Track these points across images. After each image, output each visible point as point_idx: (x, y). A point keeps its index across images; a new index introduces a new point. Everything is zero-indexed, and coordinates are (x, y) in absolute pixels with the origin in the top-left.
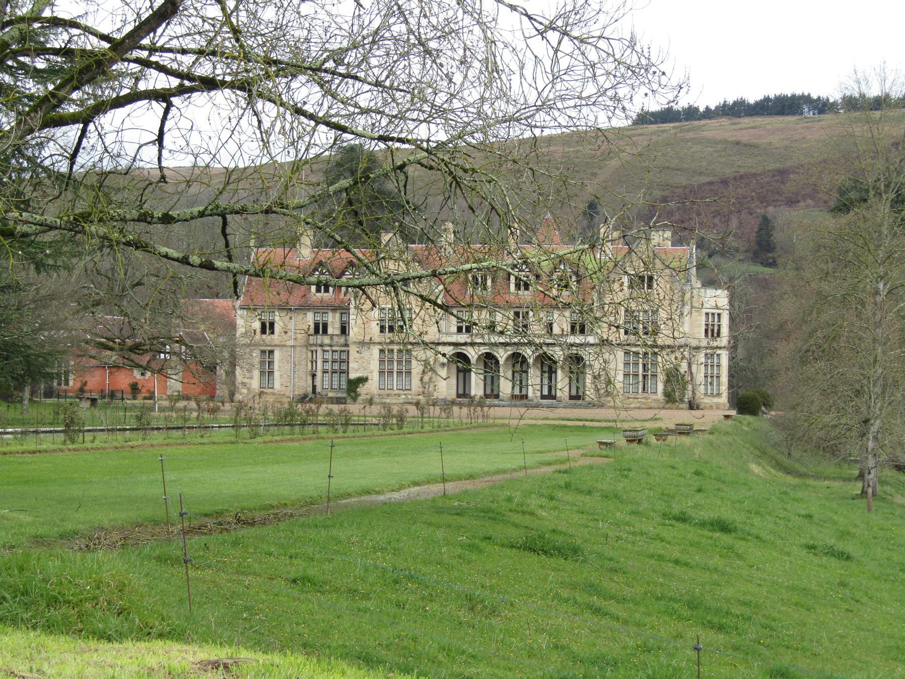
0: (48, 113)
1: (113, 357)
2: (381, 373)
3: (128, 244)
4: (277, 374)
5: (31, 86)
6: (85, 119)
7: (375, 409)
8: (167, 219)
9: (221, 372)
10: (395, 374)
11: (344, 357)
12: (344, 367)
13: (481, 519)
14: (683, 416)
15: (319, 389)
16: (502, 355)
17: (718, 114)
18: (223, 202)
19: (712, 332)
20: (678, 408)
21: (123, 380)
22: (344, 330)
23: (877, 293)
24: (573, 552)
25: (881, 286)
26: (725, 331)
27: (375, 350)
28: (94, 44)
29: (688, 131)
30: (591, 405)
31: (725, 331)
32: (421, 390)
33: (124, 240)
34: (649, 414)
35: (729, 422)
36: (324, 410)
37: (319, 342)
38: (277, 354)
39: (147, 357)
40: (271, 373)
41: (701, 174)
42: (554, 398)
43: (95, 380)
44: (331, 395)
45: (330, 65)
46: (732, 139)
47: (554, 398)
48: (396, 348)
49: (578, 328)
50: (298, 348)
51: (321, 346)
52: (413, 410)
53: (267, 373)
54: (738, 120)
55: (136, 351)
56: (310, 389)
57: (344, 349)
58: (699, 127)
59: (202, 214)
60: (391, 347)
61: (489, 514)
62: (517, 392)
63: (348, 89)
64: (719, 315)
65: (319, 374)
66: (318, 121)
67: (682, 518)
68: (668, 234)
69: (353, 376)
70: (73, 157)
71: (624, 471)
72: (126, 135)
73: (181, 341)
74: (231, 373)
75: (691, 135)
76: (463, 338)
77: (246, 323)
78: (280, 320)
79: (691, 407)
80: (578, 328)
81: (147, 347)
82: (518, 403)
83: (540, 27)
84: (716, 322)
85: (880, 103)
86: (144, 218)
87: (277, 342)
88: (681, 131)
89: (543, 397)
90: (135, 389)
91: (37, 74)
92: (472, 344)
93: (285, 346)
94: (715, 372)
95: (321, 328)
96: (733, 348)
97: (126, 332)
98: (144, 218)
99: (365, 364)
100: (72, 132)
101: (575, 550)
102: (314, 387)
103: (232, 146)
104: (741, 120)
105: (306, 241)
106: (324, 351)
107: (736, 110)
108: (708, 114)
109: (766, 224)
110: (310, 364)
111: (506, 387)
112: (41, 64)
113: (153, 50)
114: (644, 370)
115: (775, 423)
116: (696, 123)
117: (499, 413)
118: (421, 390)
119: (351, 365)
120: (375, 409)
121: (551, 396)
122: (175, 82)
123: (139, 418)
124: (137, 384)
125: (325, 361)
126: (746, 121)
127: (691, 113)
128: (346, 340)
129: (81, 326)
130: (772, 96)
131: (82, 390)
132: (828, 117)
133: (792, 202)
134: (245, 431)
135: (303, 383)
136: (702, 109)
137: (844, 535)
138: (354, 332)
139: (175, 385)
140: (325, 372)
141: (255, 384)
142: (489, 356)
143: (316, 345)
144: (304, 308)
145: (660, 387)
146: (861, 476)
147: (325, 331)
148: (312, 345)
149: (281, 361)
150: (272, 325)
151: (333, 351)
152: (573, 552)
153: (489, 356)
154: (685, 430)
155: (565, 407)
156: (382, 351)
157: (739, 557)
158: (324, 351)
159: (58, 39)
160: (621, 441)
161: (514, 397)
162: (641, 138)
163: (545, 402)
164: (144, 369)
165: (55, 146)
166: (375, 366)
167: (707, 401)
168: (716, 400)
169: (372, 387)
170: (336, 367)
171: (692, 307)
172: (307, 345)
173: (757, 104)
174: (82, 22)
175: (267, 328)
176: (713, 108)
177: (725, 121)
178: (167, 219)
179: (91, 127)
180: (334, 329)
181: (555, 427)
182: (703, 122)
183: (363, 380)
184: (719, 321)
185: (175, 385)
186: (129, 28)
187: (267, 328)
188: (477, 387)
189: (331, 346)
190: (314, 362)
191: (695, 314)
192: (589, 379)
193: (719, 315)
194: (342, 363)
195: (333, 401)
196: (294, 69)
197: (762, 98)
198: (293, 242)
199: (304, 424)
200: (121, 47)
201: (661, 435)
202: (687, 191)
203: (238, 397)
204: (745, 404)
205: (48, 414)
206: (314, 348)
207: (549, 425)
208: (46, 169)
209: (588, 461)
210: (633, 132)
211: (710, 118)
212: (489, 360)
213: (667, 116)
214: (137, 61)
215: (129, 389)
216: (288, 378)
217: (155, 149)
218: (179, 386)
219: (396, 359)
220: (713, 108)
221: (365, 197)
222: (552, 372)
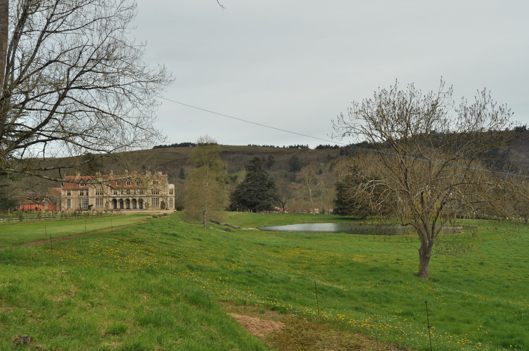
0: (15, 146)
1: (31, 202)
2: (96, 204)
5: (10, 139)
6: (25, 147)
7: (95, 212)
8: (46, 169)
9: (58, 204)
13: (120, 235)
14: (165, 211)
18: (59, 166)
21: (33, 207)
22: (87, 194)
24: (142, 242)
26: (174, 193)
27: (95, 199)
28: (25, 129)
30: (145, 210)
31: (174, 193)
34: (157, 211)
36: (83, 213)
38: (71, 200)
39: (39, 202)
40: (70, 205)
43: (26, 207)
45: (84, 133)
52: (104, 212)
53: (69, 204)
55: (37, 200)
59: (54, 168)
61: (123, 235)
63: (89, 139)
67: (167, 234)
69: (89, 204)
70: (22, 156)
71: (152, 224)
72: (35, 151)
73: (48, 197)
74: (60, 204)
76: (115, 196)
77: (64, 193)
78: (72, 192)
85: (206, 145)
86: (40, 169)
90: (36, 209)
91: (12, 136)
96: (175, 197)
97: (34, 195)
98: (40, 169)
99: (92, 201)
100: (22, 150)
101: (143, 242)
103: (61, 152)
105: (79, 174)
107: (175, 146)
109: (182, 170)
112: (13, 134)
113: (42, 131)
115: (185, 212)
117: (124, 212)
120: (95, 212)
121: (135, 208)
122: (47, 138)
123: (38, 215)
126: (177, 148)
129: (22, 194)
131: (23, 209)
132: (195, 148)
133: (188, 165)
134: (64, 218)
137: (200, 236)
138: (90, 194)
139: (46, 207)
141: (66, 207)
142: (121, 199)
144: (77, 190)
145: (160, 206)
146: (203, 223)
152: (142, 242)
153: (121, 199)
154: (165, 215)
157: (179, 242)
159: (18, 129)
160: (151, 217)
164: (39, 204)
165: (16, 154)
166: (95, 202)
169: (94, 207)
172: (79, 198)
174: (24, 124)
175: (69, 194)
177: (173, 148)
178: (46, 169)
179: (27, 149)
180: (85, 194)
183: (92, 205)
185: (46, 207)
186: (36, 126)
187: (69, 194)
188: (118, 207)
194: (87, 201)
195: (85, 210)
196: (76, 135)
198: (75, 175)
199: (78, 216)
200: (34, 130)
201: (160, 216)
203: (62, 210)
205: (15, 215)
208: (14, 158)
209: (144, 222)
213: (161, 147)
214: (38, 133)
216: (74, 205)
217: (42, 153)
218: (47, 208)
219: (99, 201)
221: (91, 164)
222: (129, 203)
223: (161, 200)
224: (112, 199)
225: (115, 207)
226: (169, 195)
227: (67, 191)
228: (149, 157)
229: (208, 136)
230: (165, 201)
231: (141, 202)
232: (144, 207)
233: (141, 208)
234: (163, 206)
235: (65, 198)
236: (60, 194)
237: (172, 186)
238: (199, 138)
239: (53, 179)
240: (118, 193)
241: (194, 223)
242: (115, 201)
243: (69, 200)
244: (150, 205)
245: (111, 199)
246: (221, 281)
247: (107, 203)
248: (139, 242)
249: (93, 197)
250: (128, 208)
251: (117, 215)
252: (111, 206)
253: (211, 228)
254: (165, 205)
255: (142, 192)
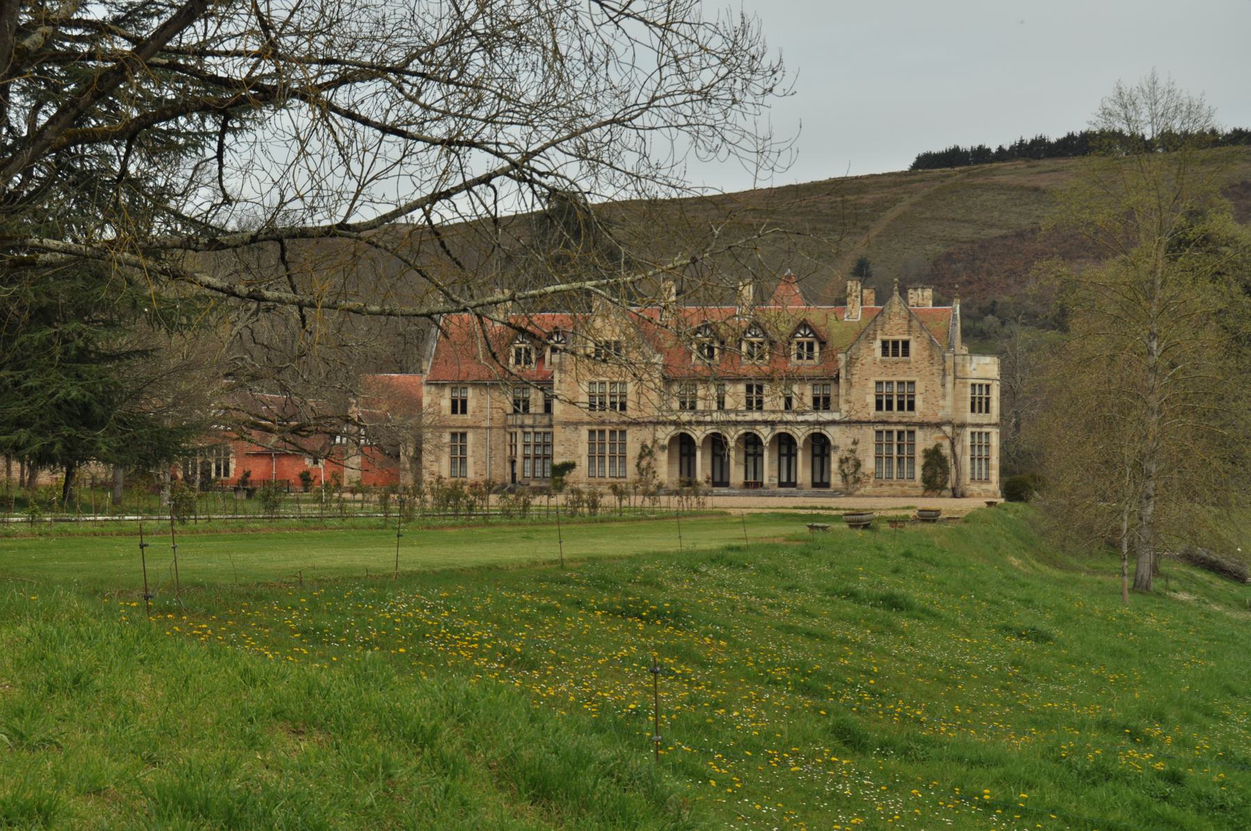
2: (591, 458)
3: (164, 272)
4: (470, 461)
10: (607, 459)
11: (548, 440)
12: (548, 452)
14: (943, 504)
15: (519, 478)
16: (732, 436)
17: (1013, 155)
19: (981, 405)
20: (939, 496)
21: (292, 469)
22: (548, 408)
23: (1150, 353)
25: (1155, 345)
26: (995, 404)
27: (584, 432)
29: (978, 175)
30: (837, 493)
31: (995, 404)
32: (637, 477)
33: (159, 268)
35: (992, 509)
37: (519, 422)
38: (470, 437)
40: (463, 460)
41: (991, 226)
42: (794, 485)
44: (533, 484)
46: (1030, 184)
47: (794, 485)
48: (608, 428)
49: (822, 403)
50: (495, 431)
51: (522, 427)
53: (459, 460)
54: (1036, 162)
55: (297, 433)
56: (509, 478)
57: (548, 430)
58: (991, 170)
60: (602, 428)
62: (751, 479)
64: (988, 386)
65: (519, 460)
66: (385, 129)
68: (929, 293)
69: (558, 461)
74: (417, 459)
75: (980, 181)
76: (686, 417)
77: (436, 402)
78: (471, 394)
79: (955, 496)
80: (822, 403)
81: (313, 428)
82: (751, 491)
83: (613, 14)
84: (984, 395)
87: (470, 423)
88: (969, 176)
89: (781, 485)
92: (699, 423)
93: (479, 427)
94: (984, 453)
95: (521, 406)
96: (1001, 425)
99: (572, 446)
102: (514, 475)
104: (1041, 162)
106: (525, 433)
108: (1002, 154)
110: (508, 448)
111: (737, 474)
114: (899, 452)
116: (987, 166)
117: (717, 501)
118: (637, 477)
119: (556, 449)
121: (790, 483)
124: (308, 473)
125: (526, 445)
126: (1046, 163)
127: (981, 154)
128: (551, 420)
130: (1077, 134)
135: (500, 471)
136: (994, 150)
140: (526, 457)
143: (515, 426)
145: (918, 473)
147: (526, 409)
148: (510, 426)
149: (474, 445)
150: (464, 402)
151: (536, 433)
154: (928, 517)
155: (806, 496)
156: (592, 432)
158: (525, 433)
161: (747, 485)
162: (922, 184)
163: (783, 490)
166: (583, 449)
167: (975, 488)
168: (985, 486)
170: (539, 451)
171: (955, 378)
173: (1060, 142)
175: (459, 406)
176: (1007, 148)
177: (1021, 164)
180: (537, 405)
181: (784, 516)
182: (995, 165)
183: (570, 466)
184: (988, 393)
187: (459, 406)
189: (533, 427)
190: (513, 446)
191: (959, 386)
192: (834, 466)
193: (988, 386)
197: (1065, 135)
202: (976, 247)
204: (1014, 490)
206: (514, 430)
207: (778, 514)
210: (912, 178)
211: (1004, 160)
212: (717, 443)
215: (299, 482)
219: (606, 442)
220: (1007, 148)
223: (924, 441)
224: (672, 431)
225: (688, 483)
226: (970, 417)
227: (447, 392)
228: (891, 214)
229: (1162, 83)
230: (946, 450)
231: (820, 446)
232: (835, 480)
233: (821, 484)
234: (937, 472)
235: (439, 427)
236: (419, 403)
237: (985, 367)
238: (1111, 93)
239: (242, 289)
240: (700, 405)
241: (1094, 571)
242: (684, 446)
243: (459, 437)
244: (869, 465)
245: (665, 435)
246: (989, 807)
247: (646, 452)
248: (659, 614)
249: (577, 424)
250: (753, 485)
251: (678, 515)
252: (665, 470)
253: (1183, 596)
254: (946, 472)
255: (827, 400)
